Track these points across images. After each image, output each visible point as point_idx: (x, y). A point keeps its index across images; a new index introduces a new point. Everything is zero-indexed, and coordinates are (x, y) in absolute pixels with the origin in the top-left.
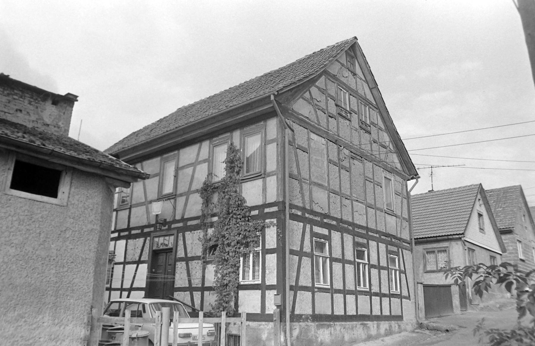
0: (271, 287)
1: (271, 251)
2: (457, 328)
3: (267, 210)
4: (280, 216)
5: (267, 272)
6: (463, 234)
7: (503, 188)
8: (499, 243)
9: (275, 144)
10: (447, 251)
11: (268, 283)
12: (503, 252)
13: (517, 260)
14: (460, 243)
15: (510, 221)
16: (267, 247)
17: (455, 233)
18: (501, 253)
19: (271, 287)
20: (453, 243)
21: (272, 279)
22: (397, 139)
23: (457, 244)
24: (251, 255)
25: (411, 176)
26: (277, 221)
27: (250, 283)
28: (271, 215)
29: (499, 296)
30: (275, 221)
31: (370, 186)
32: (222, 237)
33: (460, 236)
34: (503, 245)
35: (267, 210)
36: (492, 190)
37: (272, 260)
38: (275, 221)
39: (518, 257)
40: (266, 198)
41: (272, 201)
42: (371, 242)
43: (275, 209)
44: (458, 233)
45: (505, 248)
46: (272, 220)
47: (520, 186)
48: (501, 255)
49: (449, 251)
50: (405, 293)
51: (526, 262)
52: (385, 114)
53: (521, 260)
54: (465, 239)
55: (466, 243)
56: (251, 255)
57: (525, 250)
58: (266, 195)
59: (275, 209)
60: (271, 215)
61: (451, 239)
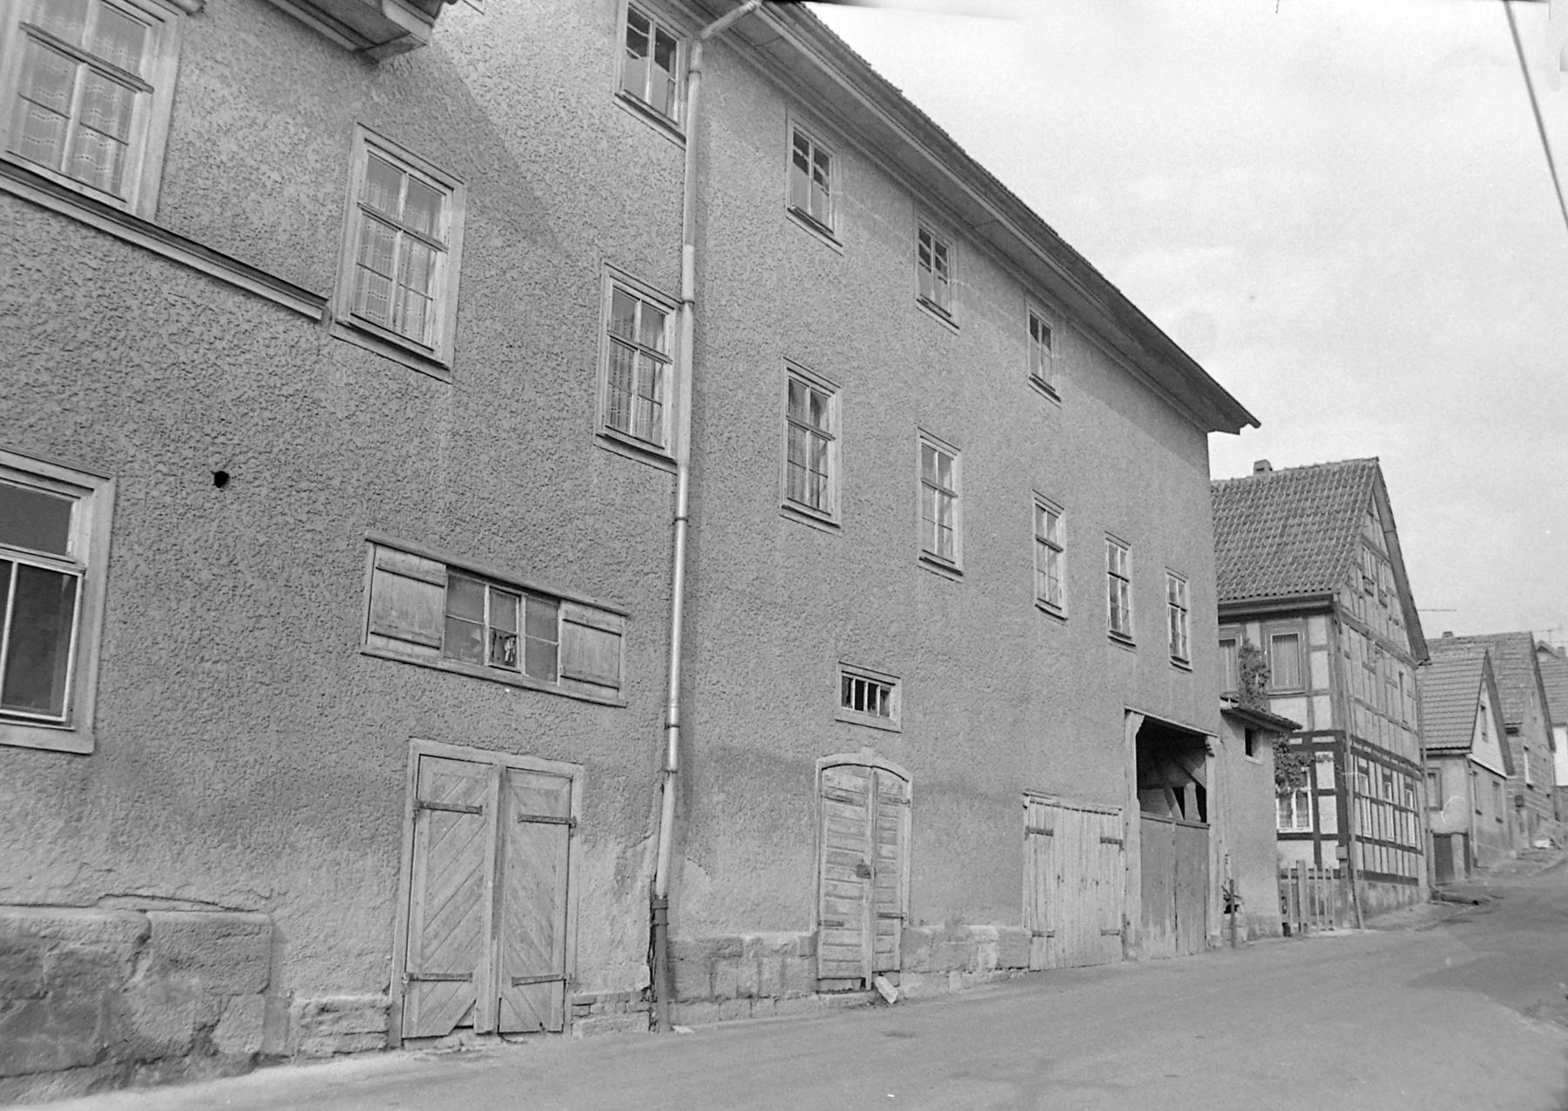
0: (1329, 837)
1: (1327, 793)
2: (1490, 898)
3: (1316, 740)
4: (1338, 749)
5: (1322, 818)
6: (1469, 748)
7: (1494, 636)
8: (1504, 757)
9: (1326, 653)
10: (1437, 776)
11: (1323, 832)
12: (1508, 774)
13: (1523, 787)
14: (1460, 762)
15: (1515, 710)
16: (1320, 787)
17: (1455, 745)
18: (1504, 774)
19: (1329, 837)
20: (1449, 762)
21: (1330, 826)
22: (1410, 607)
23: (1456, 764)
24: (1294, 795)
25: (1419, 662)
26: (1335, 755)
27: (1295, 831)
28: (1324, 747)
29: (1503, 855)
30: (1331, 754)
31: (1389, 686)
32: (195, 612)
33: (1464, 751)
34: (1511, 763)
35: (1316, 740)
36: (1472, 637)
37: (1329, 805)
38: (1331, 754)
39: (1524, 780)
40: (1313, 724)
41: (1324, 728)
42: (1395, 774)
43: (1330, 739)
44: (1460, 745)
45: (1513, 768)
46: (1326, 753)
47: (1531, 633)
48: (1505, 778)
49: (1441, 775)
50: (1419, 848)
51: (1536, 789)
52: (1399, 571)
53: (1530, 786)
54: (1471, 756)
55: (1472, 764)
56: (1294, 795)
57: (1533, 766)
58: (1313, 720)
59: (1330, 739)
60: (1324, 747)
61: (1445, 756)
